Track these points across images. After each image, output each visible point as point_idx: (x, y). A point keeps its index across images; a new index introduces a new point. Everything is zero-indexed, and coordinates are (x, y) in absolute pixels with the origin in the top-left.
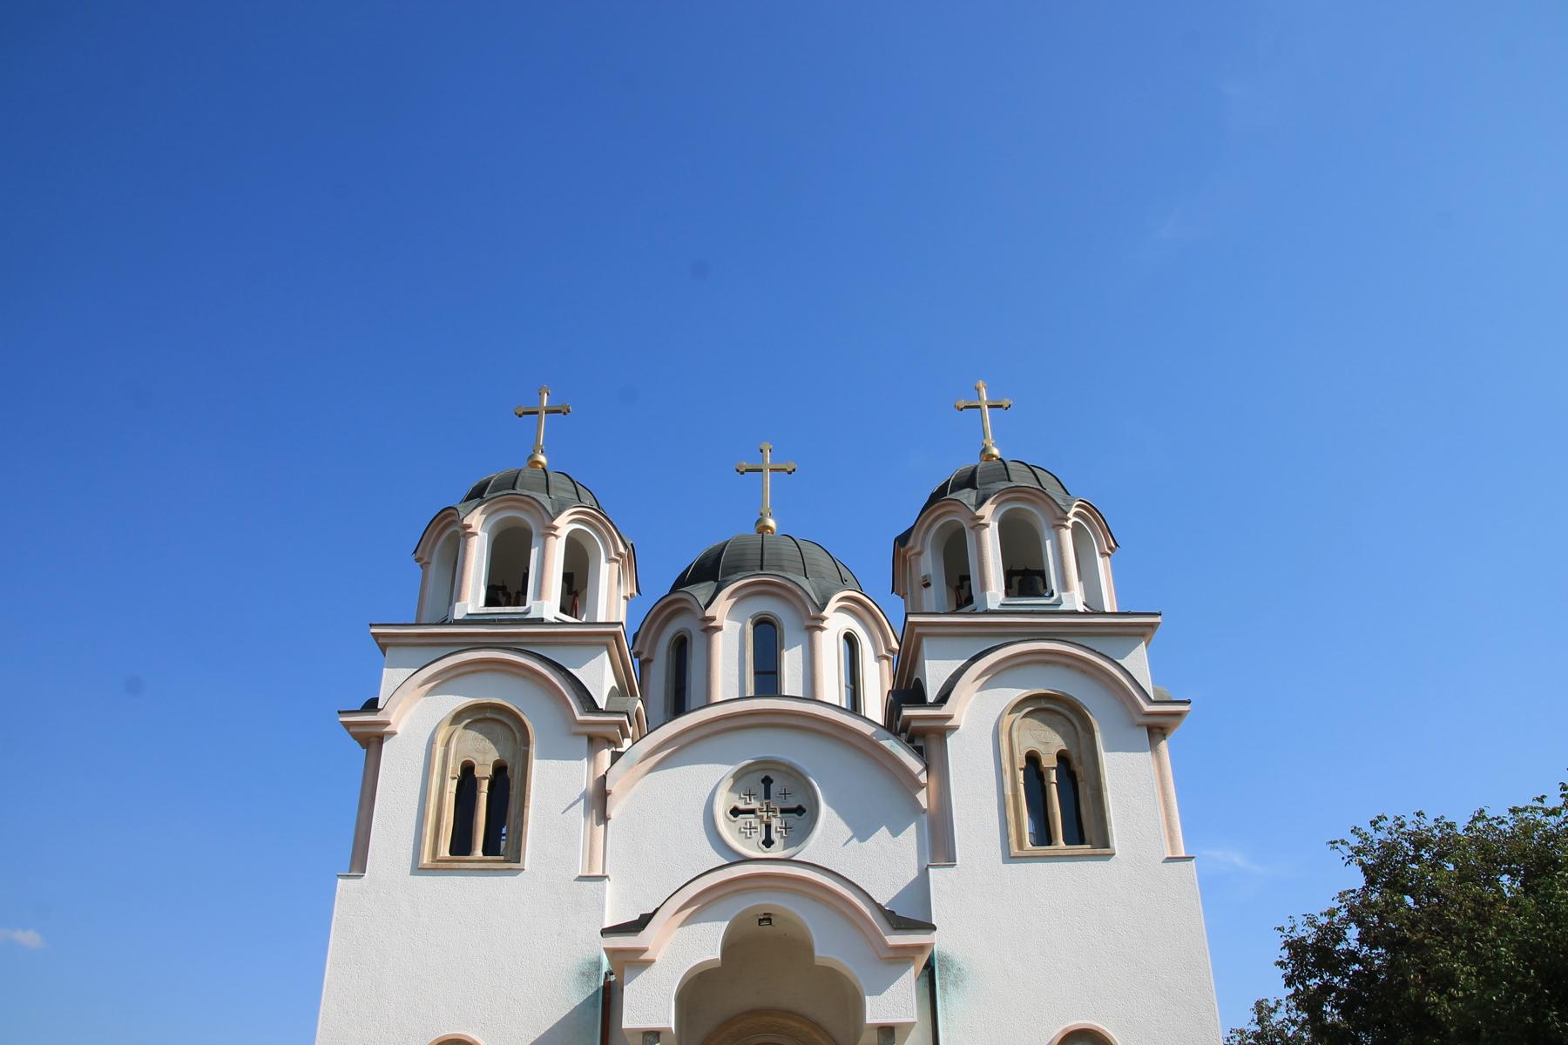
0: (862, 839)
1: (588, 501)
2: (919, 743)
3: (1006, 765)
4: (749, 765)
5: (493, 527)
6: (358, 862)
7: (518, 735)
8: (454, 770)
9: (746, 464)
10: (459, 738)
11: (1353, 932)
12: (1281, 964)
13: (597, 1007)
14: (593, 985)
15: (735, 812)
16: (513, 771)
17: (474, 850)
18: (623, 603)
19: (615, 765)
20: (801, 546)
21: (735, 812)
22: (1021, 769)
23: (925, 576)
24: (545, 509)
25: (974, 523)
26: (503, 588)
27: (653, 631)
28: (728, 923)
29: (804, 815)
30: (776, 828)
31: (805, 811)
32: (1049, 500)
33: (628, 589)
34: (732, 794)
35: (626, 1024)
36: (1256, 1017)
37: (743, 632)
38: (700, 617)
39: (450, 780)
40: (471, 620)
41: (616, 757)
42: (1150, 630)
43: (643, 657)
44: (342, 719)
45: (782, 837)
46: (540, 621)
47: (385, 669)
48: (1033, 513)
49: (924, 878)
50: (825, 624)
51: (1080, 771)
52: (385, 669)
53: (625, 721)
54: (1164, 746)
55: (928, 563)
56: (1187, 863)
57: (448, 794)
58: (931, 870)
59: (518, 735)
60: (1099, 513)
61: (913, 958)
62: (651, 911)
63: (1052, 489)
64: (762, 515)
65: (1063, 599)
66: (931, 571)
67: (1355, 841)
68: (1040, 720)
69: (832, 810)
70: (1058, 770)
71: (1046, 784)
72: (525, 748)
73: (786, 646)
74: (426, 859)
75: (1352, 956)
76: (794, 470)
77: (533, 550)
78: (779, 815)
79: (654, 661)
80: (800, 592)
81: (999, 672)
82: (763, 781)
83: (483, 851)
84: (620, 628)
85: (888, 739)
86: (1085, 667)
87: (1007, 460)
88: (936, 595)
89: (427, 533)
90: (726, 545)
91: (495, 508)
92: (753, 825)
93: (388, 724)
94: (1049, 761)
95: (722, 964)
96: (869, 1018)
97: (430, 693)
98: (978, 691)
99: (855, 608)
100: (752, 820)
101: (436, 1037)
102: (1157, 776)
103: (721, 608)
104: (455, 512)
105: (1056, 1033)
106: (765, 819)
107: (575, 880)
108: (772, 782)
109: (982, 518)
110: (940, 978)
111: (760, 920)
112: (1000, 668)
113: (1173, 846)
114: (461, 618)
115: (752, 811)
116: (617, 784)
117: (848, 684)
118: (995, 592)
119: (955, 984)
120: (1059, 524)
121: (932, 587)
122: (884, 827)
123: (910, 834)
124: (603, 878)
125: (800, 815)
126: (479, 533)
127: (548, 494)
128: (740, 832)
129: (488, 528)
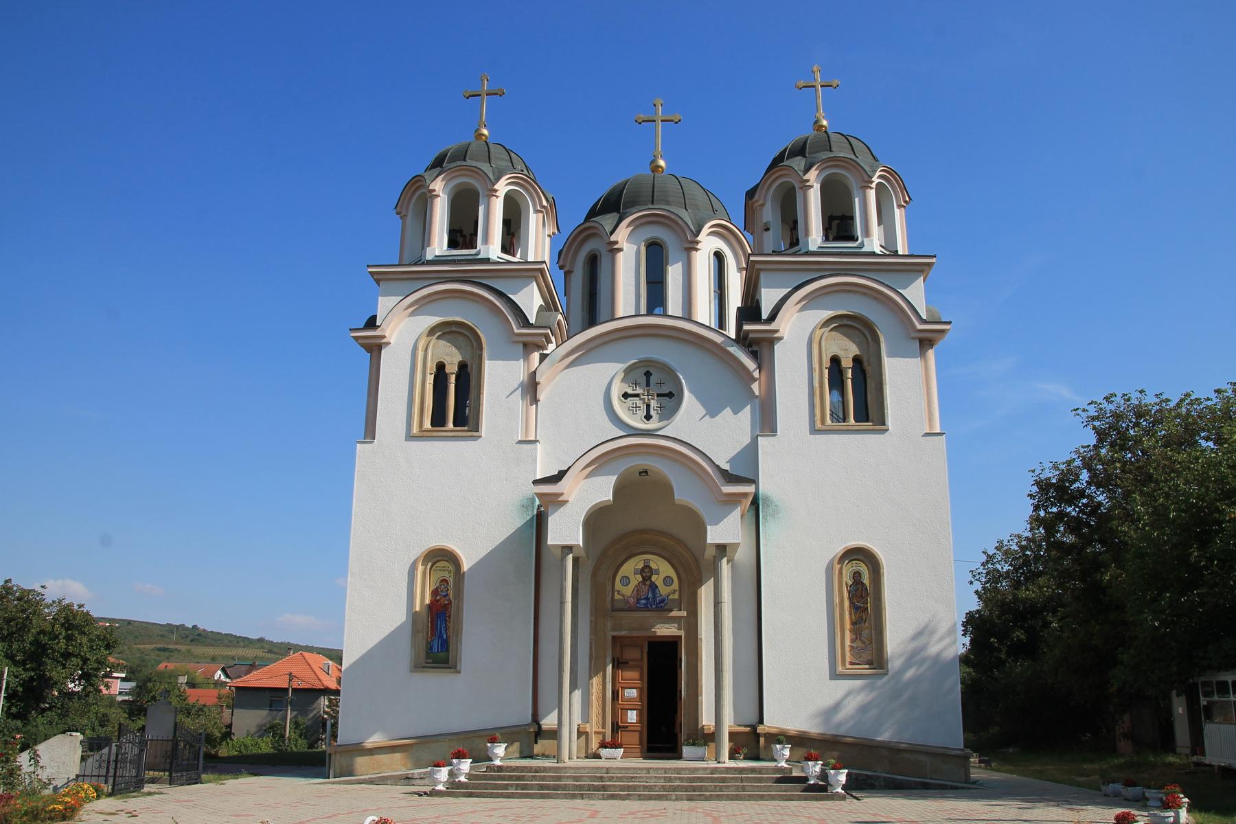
0: (713, 416)
2: (755, 348)
3: (816, 365)
4: (635, 363)
6: (370, 432)
7: (475, 344)
8: (431, 369)
9: (642, 116)
10: (434, 346)
11: (1085, 476)
12: (1030, 496)
13: (533, 528)
15: (626, 396)
18: (548, 240)
20: (682, 184)
21: (626, 396)
23: (766, 223)
24: (487, 176)
27: (571, 252)
31: (674, 395)
32: (859, 168)
33: (550, 229)
34: (623, 384)
35: (550, 542)
37: (638, 252)
41: (543, 357)
43: (567, 268)
45: (658, 413)
46: (487, 261)
47: (380, 298)
51: (869, 369)
52: (380, 298)
53: (548, 333)
54: (931, 353)
55: (769, 213)
58: (759, 438)
59: (475, 344)
60: (897, 174)
62: (566, 469)
63: (864, 160)
64: (654, 156)
66: (770, 219)
67: (1092, 411)
68: (841, 333)
70: (853, 369)
71: (844, 379)
74: (415, 430)
75: (1082, 493)
76: (680, 121)
78: (656, 398)
79: (575, 271)
81: (815, 297)
82: (645, 374)
87: (829, 132)
90: (624, 187)
92: (638, 405)
93: (384, 337)
94: (847, 363)
97: (412, 314)
98: (798, 312)
99: (722, 232)
100: (638, 402)
101: (427, 547)
102: (924, 375)
103: (622, 235)
104: (423, 179)
106: (646, 401)
108: (651, 374)
110: (762, 512)
111: (640, 472)
112: (817, 294)
113: (931, 426)
115: (637, 395)
117: (717, 290)
118: (815, 237)
119: (773, 515)
120: (866, 185)
121: (771, 230)
123: (746, 412)
124: (535, 442)
125: (670, 398)
126: (441, 195)
127: (490, 163)
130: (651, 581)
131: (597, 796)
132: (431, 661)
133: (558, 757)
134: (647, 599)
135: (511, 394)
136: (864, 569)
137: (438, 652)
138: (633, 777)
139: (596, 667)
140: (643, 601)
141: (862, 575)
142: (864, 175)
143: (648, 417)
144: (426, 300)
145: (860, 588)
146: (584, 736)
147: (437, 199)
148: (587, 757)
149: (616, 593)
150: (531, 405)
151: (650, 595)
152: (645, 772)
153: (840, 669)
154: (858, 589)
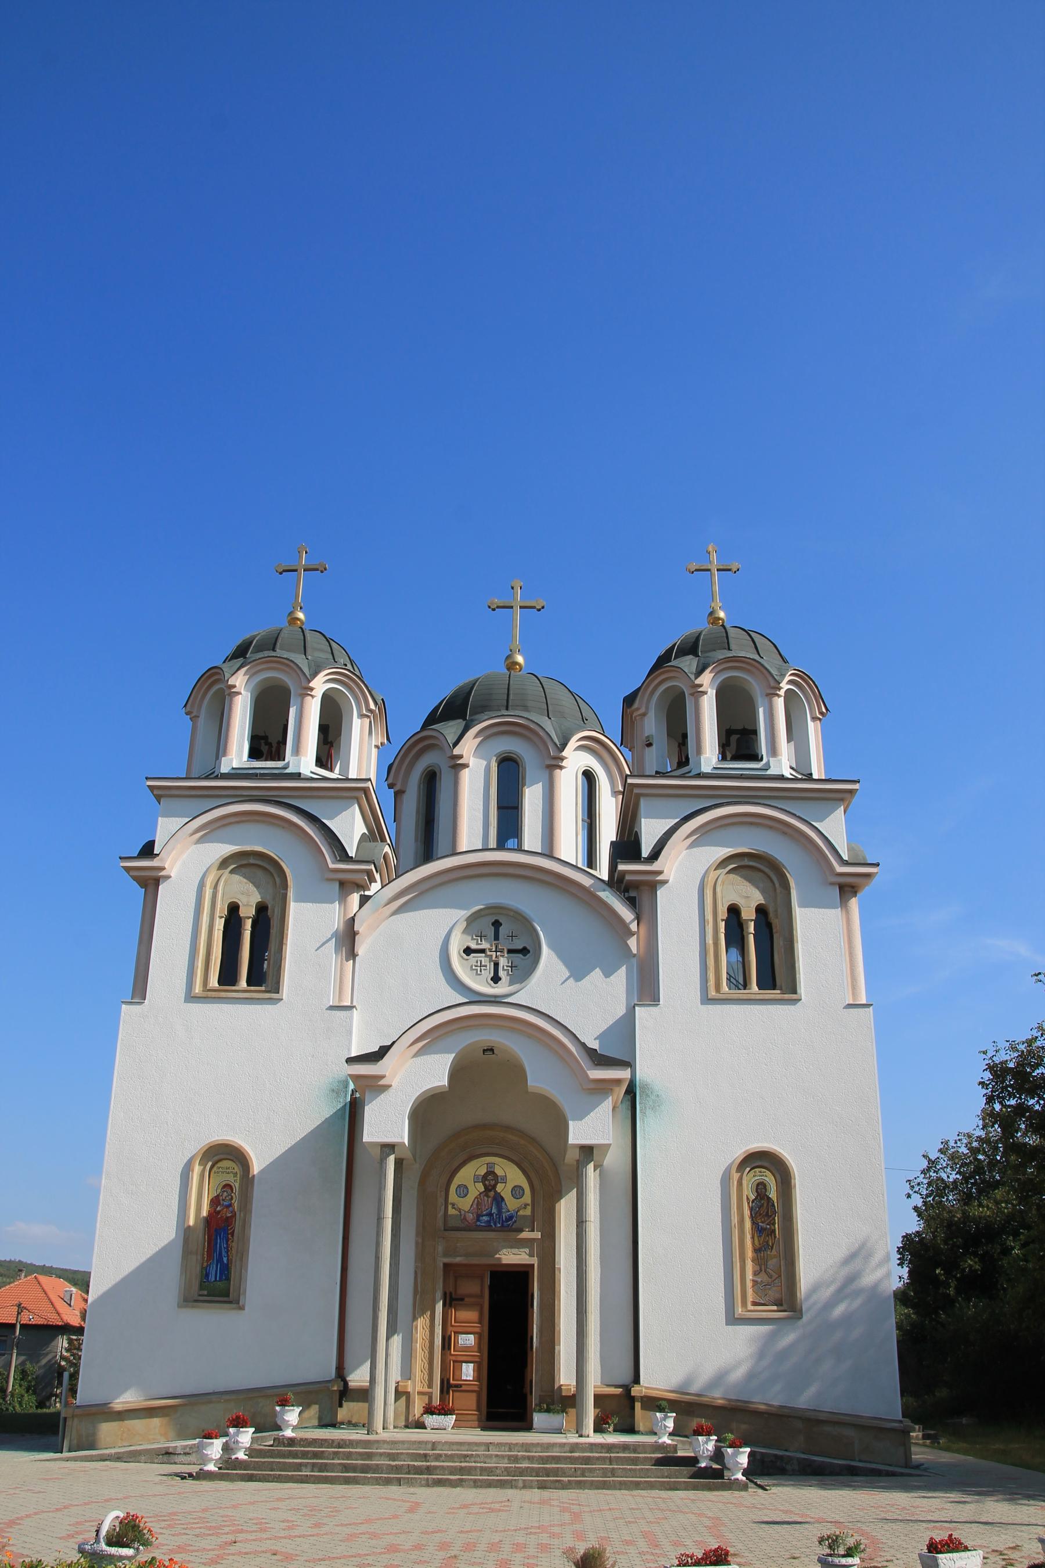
1: (342, 659)
2: (632, 894)
3: (709, 917)
4: (481, 910)
5: (257, 685)
6: (139, 990)
7: (278, 880)
9: (497, 601)
10: (226, 882)
12: (982, 1084)
14: (341, 1100)
15: (468, 951)
16: (274, 912)
17: (239, 980)
18: (374, 751)
19: (363, 908)
21: (468, 951)
22: (722, 920)
23: (648, 737)
25: (693, 691)
26: (265, 738)
28: (454, 1055)
30: (503, 967)
31: (529, 952)
33: (379, 738)
35: (366, 1138)
36: (981, 1123)
37: (488, 769)
38: (449, 755)
39: (218, 919)
40: (236, 774)
41: (364, 900)
42: (847, 796)
43: (398, 787)
44: (123, 864)
45: (508, 974)
46: (297, 776)
47: (160, 818)
48: (749, 681)
49: (629, 1019)
50: (564, 764)
51: (776, 923)
52: (160, 818)
53: (372, 870)
54: (854, 903)
55: (652, 725)
56: (866, 1009)
57: (216, 931)
59: (278, 880)
61: (611, 1089)
62: (390, 1044)
63: (770, 661)
64: (511, 651)
65: (771, 765)
68: (741, 877)
69: (552, 953)
70: (756, 921)
71: (745, 934)
72: (283, 891)
73: (527, 784)
74: (198, 989)
76: (543, 607)
77: (291, 710)
78: (506, 955)
80: (542, 733)
81: (706, 832)
82: (493, 924)
83: (247, 982)
84: (369, 784)
85: (604, 891)
86: (785, 829)
87: (728, 626)
88: (657, 757)
89: (199, 684)
90: (474, 684)
92: (483, 963)
93: (163, 869)
94: (748, 914)
95: (449, 1088)
96: (572, 1140)
97: (199, 841)
98: (687, 849)
99: (593, 746)
101: (210, 1141)
103: (468, 748)
105: (740, 1153)
106: (494, 958)
107: (327, 1009)
108: (501, 924)
109: (701, 686)
112: (709, 828)
114: (227, 772)
115: (483, 951)
116: (364, 925)
119: (653, 1108)
120: (772, 691)
121: (654, 745)
122: (598, 968)
123: (621, 975)
124: (351, 1008)
126: (243, 692)
127: (305, 655)
130: (496, 1192)
132: (205, 1292)
134: (490, 1214)
136: (770, 1179)
138: (467, 1456)
140: (485, 1218)
141: (768, 1188)
145: (765, 1205)
146: (404, 1398)
147: (237, 697)
148: (407, 1427)
149: (450, 1207)
150: (347, 961)
151: (494, 1210)
152: (483, 1448)
154: (763, 1204)
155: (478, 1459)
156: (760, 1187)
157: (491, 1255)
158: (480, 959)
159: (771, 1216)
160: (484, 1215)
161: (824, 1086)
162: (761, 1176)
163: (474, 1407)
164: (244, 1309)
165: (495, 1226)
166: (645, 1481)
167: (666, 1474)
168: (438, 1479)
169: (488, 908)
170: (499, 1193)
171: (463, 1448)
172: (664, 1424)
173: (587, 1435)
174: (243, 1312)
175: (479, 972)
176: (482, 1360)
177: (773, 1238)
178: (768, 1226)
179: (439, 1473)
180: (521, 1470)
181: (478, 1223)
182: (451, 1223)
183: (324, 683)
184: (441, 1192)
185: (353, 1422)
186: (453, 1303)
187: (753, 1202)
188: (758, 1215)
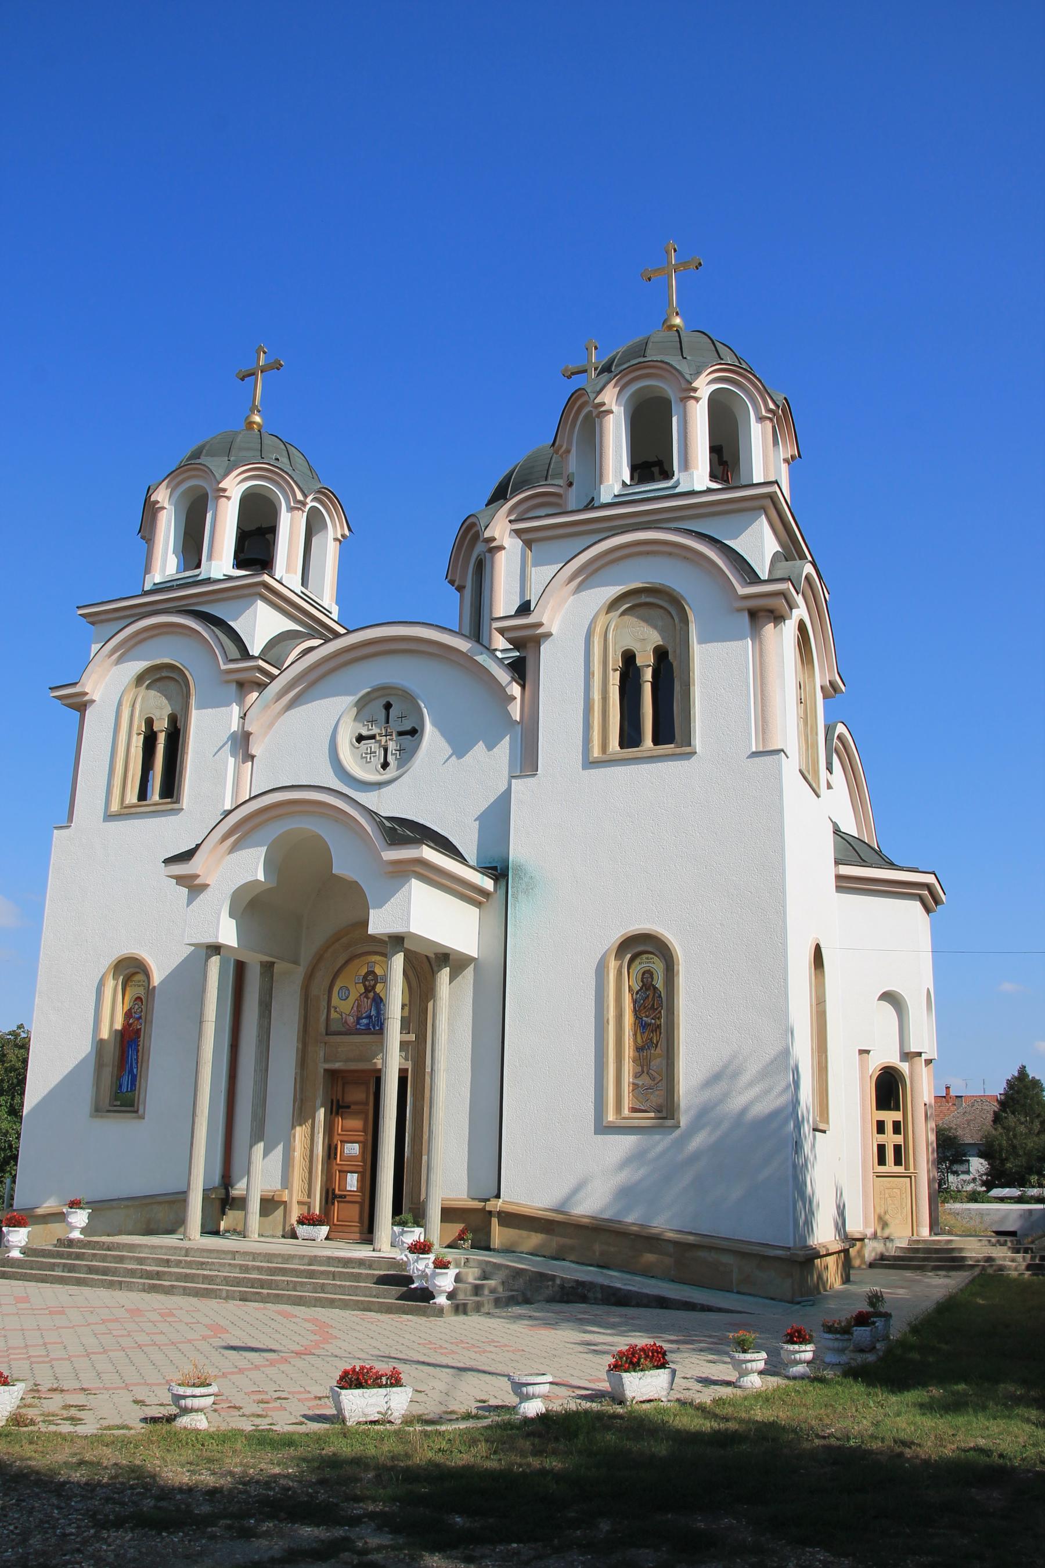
4: (368, 693)
8: (615, 661)
10: (143, 698)
15: (360, 738)
28: (266, 848)
29: (416, 735)
32: (674, 372)
39: (611, 672)
45: (396, 759)
47: (93, 645)
52: (93, 645)
68: (638, 617)
74: (596, 753)
91: (622, 382)
92: (373, 750)
97: (578, 589)
106: (383, 743)
115: (373, 737)
122: (481, 742)
123: (504, 746)
126: (615, 408)
128: (362, 758)
129: (623, 402)
130: (375, 992)
131: (250, 1285)
132: (119, 1103)
133: (243, 1234)
134: (369, 1017)
135: (215, 754)
136: (658, 966)
137: (127, 1091)
138: (203, 1263)
139: (302, 1114)
140: (365, 1021)
141: (655, 976)
142: (682, 381)
143: (385, 765)
144: (132, 642)
145: (651, 996)
146: (282, 1207)
147: (161, 512)
148: (283, 1237)
149: (332, 1010)
150: (244, 763)
151: (373, 1013)
152: (230, 1256)
153: (611, 1117)
154: (648, 996)
155: (213, 1267)
156: (646, 975)
157: (369, 1059)
158: (370, 745)
159: (656, 1009)
160: (364, 1018)
161: (719, 853)
162: (648, 963)
163: (357, 1219)
164: (144, 1118)
165: (374, 1028)
166: (340, 1299)
167: (375, 1293)
168: (153, 1284)
169: (375, 690)
170: (378, 994)
171: (212, 1255)
172: (402, 1240)
173: (378, 1249)
174: (143, 1121)
175: (368, 760)
176: (365, 1170)
177: (658, 1033)
178: (653, 1021)
179: (166, 1279)
180: (238, 1280)
181: (358, 1026)
182: (334, 1027)
183: (708, 384)
184: (324, 995)
185: (238, 1231)
186: (340, 1110)
187: (637, 993)
188: (642, 1008)
